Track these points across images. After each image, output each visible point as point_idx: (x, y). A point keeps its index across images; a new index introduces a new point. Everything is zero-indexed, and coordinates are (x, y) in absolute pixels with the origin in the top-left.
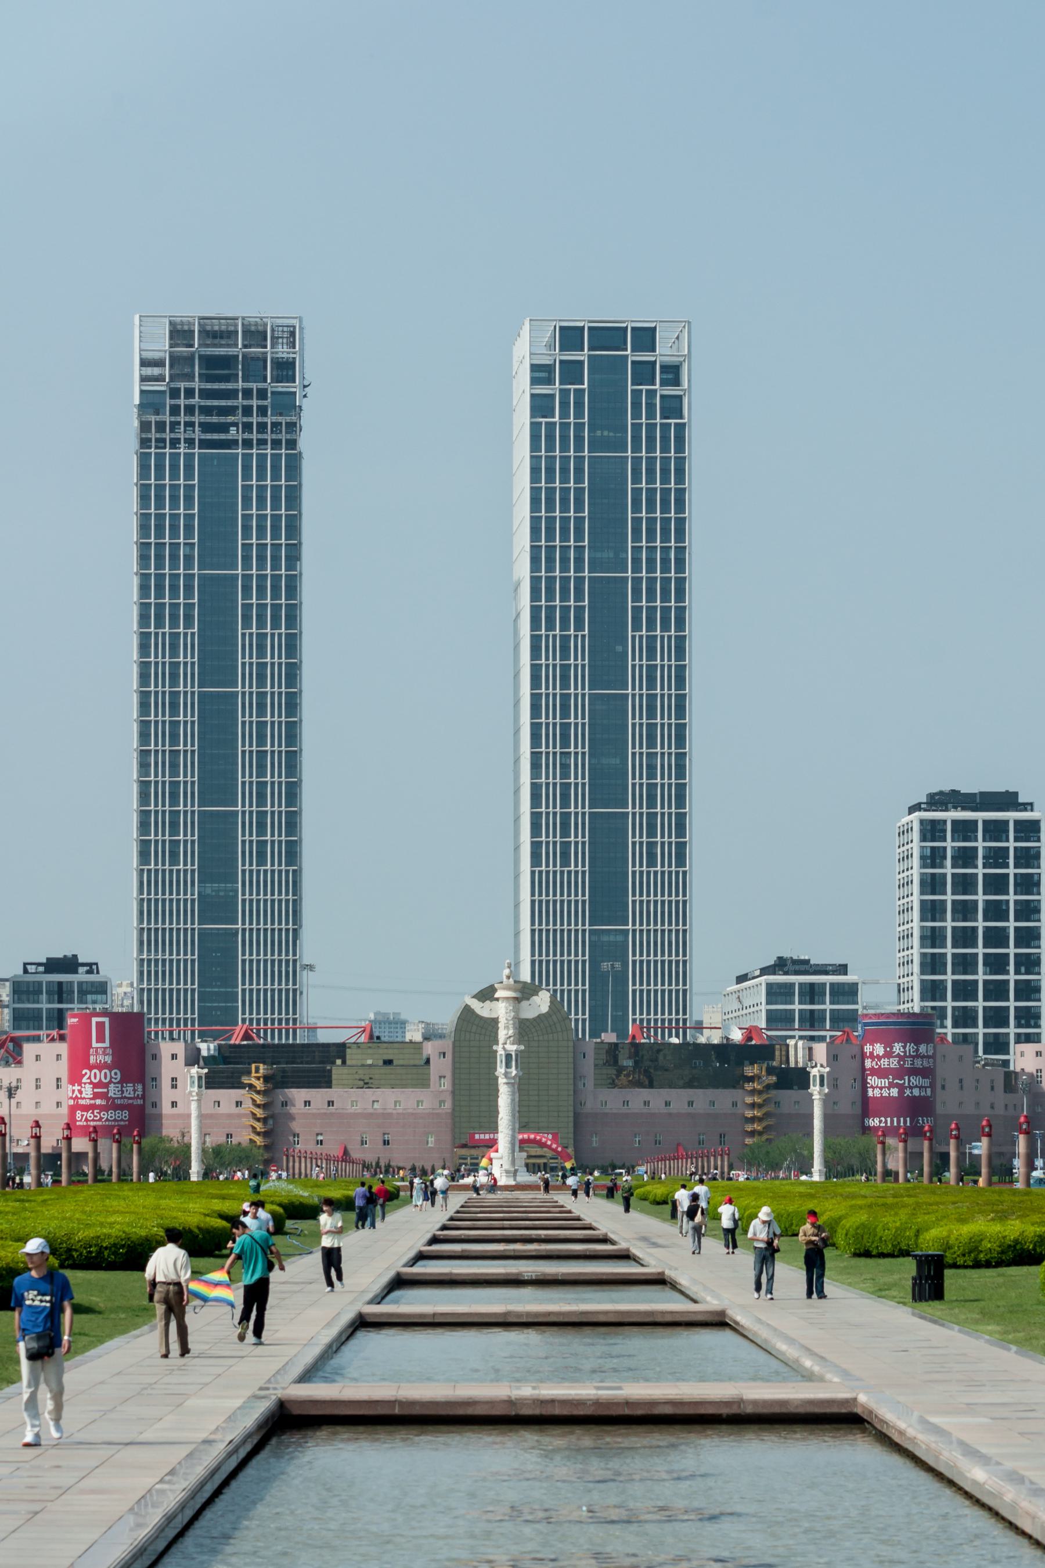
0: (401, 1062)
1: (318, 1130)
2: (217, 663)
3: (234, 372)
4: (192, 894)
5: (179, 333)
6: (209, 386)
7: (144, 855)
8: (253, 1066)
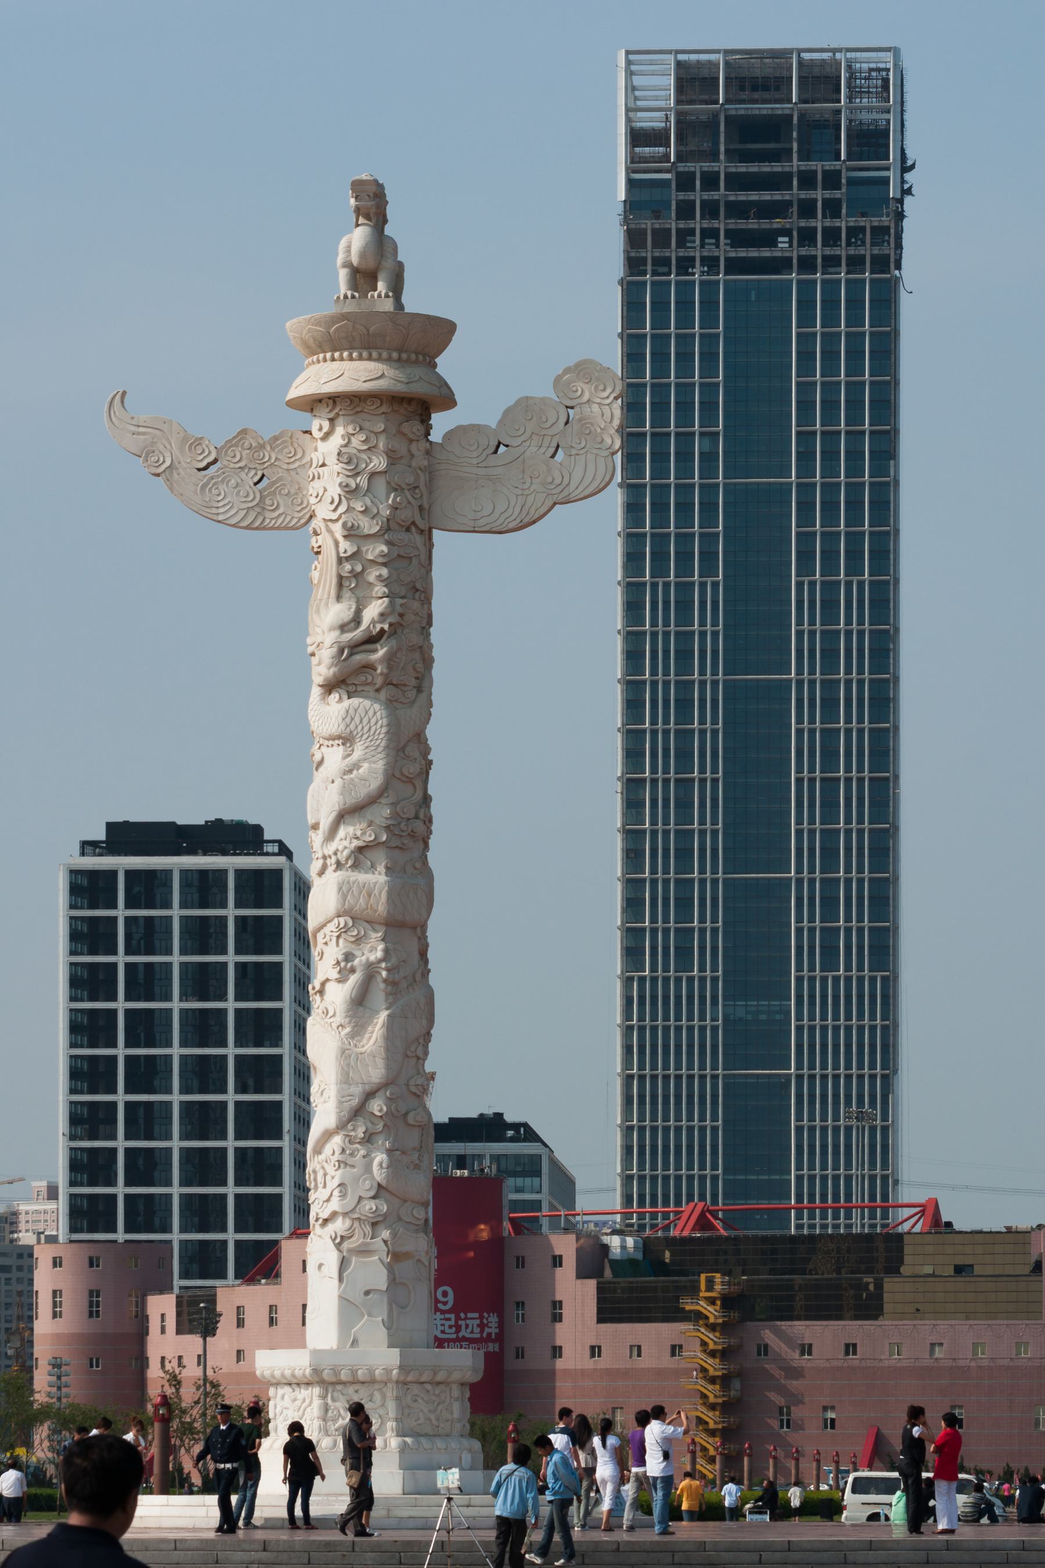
0: (989, 1270)
1: (826, 1400)
2: (755, 632)
3: (786, 146)
4: (714, 1019)
5: (693, 80)
6: (743, 168)
7: (632, 954)
8: (703, 1277)
